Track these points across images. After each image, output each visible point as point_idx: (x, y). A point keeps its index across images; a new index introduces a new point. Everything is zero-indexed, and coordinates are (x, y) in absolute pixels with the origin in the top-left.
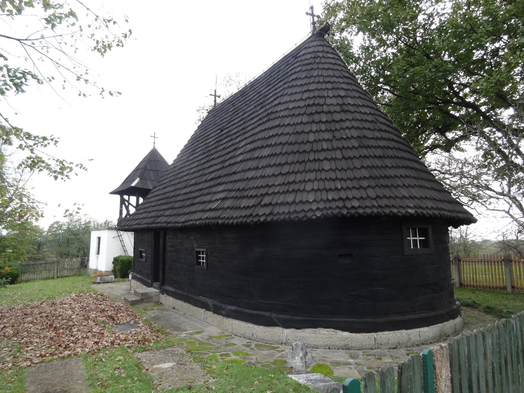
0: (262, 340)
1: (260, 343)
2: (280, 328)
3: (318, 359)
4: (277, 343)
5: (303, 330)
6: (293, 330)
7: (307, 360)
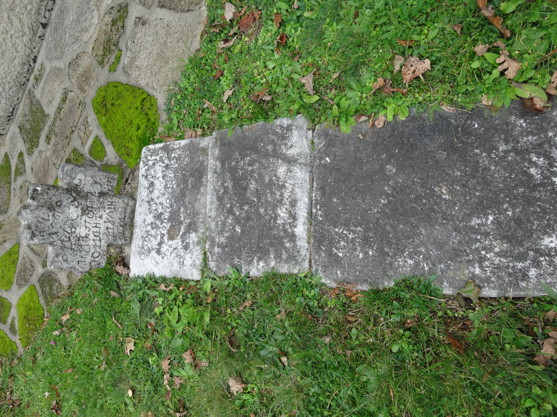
3: (76, 91)
7: (97, 189)
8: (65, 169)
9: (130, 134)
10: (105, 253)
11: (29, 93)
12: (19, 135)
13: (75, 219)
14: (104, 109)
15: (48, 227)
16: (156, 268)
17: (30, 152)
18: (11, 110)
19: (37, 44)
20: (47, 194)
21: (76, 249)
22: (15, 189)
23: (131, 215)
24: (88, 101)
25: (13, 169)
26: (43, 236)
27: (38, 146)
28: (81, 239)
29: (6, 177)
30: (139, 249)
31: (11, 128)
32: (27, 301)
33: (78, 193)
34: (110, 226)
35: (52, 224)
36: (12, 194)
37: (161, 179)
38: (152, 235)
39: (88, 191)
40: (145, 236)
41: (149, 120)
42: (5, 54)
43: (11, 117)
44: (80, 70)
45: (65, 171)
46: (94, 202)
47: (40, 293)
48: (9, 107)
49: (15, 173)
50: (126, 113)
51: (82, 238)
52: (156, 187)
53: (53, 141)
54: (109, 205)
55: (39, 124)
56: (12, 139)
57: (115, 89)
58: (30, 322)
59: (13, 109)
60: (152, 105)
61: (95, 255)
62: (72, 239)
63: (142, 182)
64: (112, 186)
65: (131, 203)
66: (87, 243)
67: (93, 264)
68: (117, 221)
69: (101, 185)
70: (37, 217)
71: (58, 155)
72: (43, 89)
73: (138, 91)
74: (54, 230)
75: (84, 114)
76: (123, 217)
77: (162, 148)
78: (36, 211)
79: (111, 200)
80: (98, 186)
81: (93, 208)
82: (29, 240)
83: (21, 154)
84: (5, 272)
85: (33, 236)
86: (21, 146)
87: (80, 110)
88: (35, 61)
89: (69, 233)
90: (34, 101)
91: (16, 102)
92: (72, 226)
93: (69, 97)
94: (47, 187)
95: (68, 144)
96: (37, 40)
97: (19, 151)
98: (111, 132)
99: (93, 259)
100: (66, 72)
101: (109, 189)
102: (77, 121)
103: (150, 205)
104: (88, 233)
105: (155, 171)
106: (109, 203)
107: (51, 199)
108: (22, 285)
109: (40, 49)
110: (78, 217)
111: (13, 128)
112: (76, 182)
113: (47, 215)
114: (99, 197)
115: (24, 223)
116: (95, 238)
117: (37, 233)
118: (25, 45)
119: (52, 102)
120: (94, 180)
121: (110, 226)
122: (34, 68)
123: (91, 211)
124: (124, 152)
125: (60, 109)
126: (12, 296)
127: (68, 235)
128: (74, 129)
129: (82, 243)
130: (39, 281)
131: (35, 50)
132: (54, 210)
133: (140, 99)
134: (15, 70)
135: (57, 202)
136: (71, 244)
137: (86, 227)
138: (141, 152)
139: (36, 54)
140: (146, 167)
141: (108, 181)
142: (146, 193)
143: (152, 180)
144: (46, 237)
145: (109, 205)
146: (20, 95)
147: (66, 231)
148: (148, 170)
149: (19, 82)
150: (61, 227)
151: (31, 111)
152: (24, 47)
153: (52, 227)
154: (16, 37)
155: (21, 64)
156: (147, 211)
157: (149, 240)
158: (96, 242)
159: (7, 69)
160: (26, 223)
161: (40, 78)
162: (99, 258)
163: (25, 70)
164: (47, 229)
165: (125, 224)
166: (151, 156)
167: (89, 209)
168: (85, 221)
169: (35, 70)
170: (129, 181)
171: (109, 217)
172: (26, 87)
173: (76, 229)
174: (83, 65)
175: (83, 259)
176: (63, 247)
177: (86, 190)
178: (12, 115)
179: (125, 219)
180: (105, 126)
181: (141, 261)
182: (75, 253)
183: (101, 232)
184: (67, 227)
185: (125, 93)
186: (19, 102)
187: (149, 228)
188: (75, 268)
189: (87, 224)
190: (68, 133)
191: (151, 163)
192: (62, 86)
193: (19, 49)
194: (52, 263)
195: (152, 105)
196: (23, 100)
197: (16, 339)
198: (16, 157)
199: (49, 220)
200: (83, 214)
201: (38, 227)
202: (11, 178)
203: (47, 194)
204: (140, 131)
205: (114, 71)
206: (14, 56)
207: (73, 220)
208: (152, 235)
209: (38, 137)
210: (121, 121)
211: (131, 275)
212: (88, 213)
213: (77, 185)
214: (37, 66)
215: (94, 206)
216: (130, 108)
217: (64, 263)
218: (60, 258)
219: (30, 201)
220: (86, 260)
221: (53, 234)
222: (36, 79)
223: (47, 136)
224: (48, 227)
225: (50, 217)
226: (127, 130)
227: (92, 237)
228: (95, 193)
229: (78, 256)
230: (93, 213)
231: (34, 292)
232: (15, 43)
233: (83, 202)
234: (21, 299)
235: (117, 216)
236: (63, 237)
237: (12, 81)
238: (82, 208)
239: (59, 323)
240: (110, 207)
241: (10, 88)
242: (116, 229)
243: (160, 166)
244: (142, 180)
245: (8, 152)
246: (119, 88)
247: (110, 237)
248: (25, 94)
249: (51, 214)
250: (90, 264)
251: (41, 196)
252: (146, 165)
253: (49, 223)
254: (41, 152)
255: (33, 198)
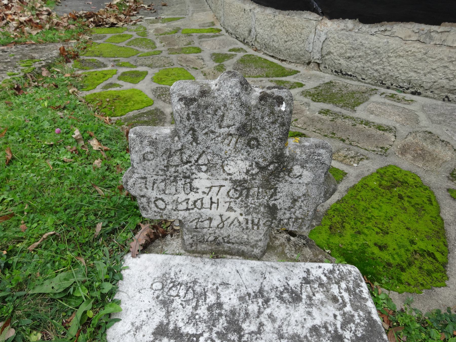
0: (266, 46)
1: (260, 55)
2: (313, 16)
3: (399, 143)
4: (298, 60)
5: (387, 26)
6: (350, 23)
7: (282, 201)
8: (322, 151)
9: (366, 231)
10: (165, 217)
11: (373, 90)
12: (322, 82)
13: (224, 171)
14: (389, 184)
15: (206, 127)
16: (128, 327)
17: (305, 94)
18: (349, 73)
19: (437, 94)
20: (273, 123)
21: (168, 174)
22: (261, 81)
23: (235, 251)
24: (392, 160)
25: (284, 79)
26: (189, 119)
27: (315, 101)
28: (188, 180)
29: (273, 73)
30: (172, 275)
31: (327, 75)
32: (137, 98)
33: (275, 174)
34: (215, 223)
35: (213, 132)
36: (255, 79)
37: (309, 324)
38: (196, 308)
39: (279, 190)
40: (198, 289)
41: (403, 270)
42: (422, 62)
43: (340, 74)
44: (430, 147)
45: (318, 151)
46: (258, 199)
47: (142, 111)
48: (353, 70)
49: (279, 81)
50: (396, 221)
51: (190, 183)
52: (291, 310)
53: (324, 117)
54: (253, 221)
55: (340, 101)
56: (316, 76)
57: (425, 200)
58: (111, 102)
59: (351, 75)
60: (429, 273)
61: (160, 203)
62: (187, 166)
63: (296, 271)
64: (287, 224)
65: (257, 251)
66: (180, 189)
67: (144, 200)
68: (224, 233)
69: (290, 208)
70: (225, 106)
71: (309, 123)
72: (384, 104)
73: (441, 243)
74: (201, 137)
75: (371, 155)
76: (233, 241)
77: (371, 322)
78: (238, 104)
79: (261, 223)
80: (288, 204)
81: (247, 196)
82: (179, 95)
83: (301, 85)
84: (173, 76)
85: (188, 101)
86: (310, 85)
87: (375, 149)
88: (413, 93)
89: (197, 161)
90: (366, 95)
91: (360, 78)
92: (210, 167)
93: (386, 134)
94: (286, 121)
95: (326, 136)
96: (443, 94)
97: (304, 83)
98: (358, 197)
99: (153, 200)
100: (418, 129)
101: (281, 220)
102: (359, 145)
103: (256, 297)
104: (200, 191)
105: (322, 303)
106: (256, 221)
107: (263, 128)
108: (156, 92)
109: (431, 98)
110: (229, 174)
111: (328, 77)
112: (297, 170)
113: (231, 123)
114: (267, 206)
115: (213, 84)
116: (190, 203)
117: (193, 107)
118: (435, 82)
119: (372, 114)
120: (300, 197)
121: (215, 223)
122: (404, 92)
123: (241, 195)
124: (334, 220)
125: (367, 123)
126: (145, 84)
127: (193, 160)
128: (347, 142)
129: (180, 183)
130: (157, 109)
131: (429, 93)
132: (240, 135)
133: (431, 249)
134: (400, 74)
135: (256, 139)
136: (177, 166)
137: (211, 188)
138: (350, 262)
139: (424, 94)
140: (324, 279)
141: (297, 219)
142: (277, 284)
143: (304, 296)
144: (187, 123)
145: (253, 221)
146: (369, 81)
147: (200, 156)
148: (321, 285)
149: (385, 78)
150: (208, 148)
151: (353, 93)
152: (433, 80)
153: (206, 133)
154: (445, 72)
155: (410, 78)
156: (243, 291)
157: (187, 301)
158: (184, 204)
159: (401, 65)
160: (213, 87)
161: (395, 99)
162: (156, 209)
163: (401, 84)
164: (203, 125)
165: (219, 244)
166: (348, 290)
167: (245, 192)
168: (221, 186)
169: (403, 94)
170: (292, 238)
171: (230, 221)
172: (379, 86)
173: (206, 172)
174: (437, 150)
175: (150, 185)
176: (169, 153)
177: (281, 185)
178: (343, 74)
179: (228, 242)
180: (364, 186)
181: (149, 281)
182: (161, 173)
183: (203, 210)
184: (209, 158)
185: (427, 217)
186: (359, 81)
187: (211, 299)
188: (134, 172)
189: (215, 189)
190: (339, 134)
191: (335, 289)
192: (397, 125)
193: (428, 76)
194: (139, 135)
195: (429, 273)
196: (363, 84)
197: (98, 90)
198: (296, 81)
199: (220, 127)
200: (234, 182)
201: (206, 108)
202: (272, 77)
203: (273, 123)
204: (376, 250)
205: (451, 197)
206: (419, 71)
207: (222, 166)
208: (196, 308)
209: (325, 101)
210: (381, 214)
211: (129, 260)
212: (236, 190)
213: (290, 171)
214: (409, 96)
215: (251, 198)
216: (408, 229)
217: (140, 154)
218: (148, 149)
219: (257, 92)
220: (150, 190)
221: (193, 135)
222: (392, 96)
223: (328, 111)
224: (206, 127)
225: (226, 129)
226: (369, 225)
227: (193, 197)
228: (275, 200)
229: (155, 177)
230: (237, 198)
231: (145, 104)
232: (437, 71)
233: (258, 181)
234: (140, 93)
235: (233, 232)
236: (188, 152)
237: (385, 72)
238: (245, 181)
239: (91, 136)
240: (250, 222)
241: (376, 70)
242: (209, 231)
243: (335, 316)
244: (299, 270)
245: (300, 73)
246: (431, 207)
247: (194, 223)
248: (370, 86)
249: (232, 130)
250: (143, 196)
251: (268, 111)
252: (329, 278)
253: (214, 127)
254: (308, 105)
255: (263, 97)
